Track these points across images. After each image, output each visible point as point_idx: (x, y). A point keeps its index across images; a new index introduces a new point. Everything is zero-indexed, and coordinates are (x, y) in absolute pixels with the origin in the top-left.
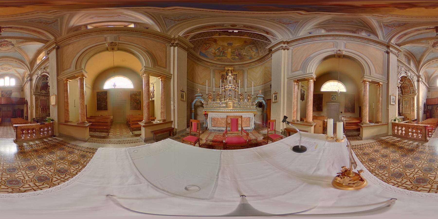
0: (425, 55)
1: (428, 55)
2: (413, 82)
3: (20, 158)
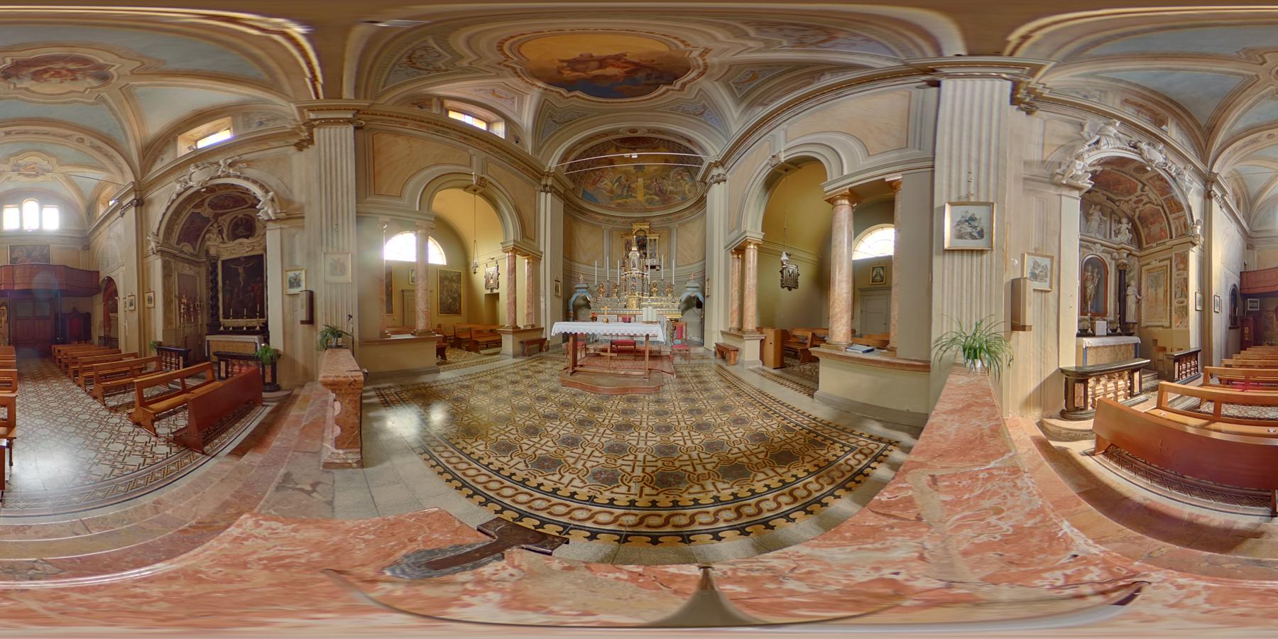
0: (1237, 104)
1: (1251, 106)
2: (1182, 191)
3: (686, 457)
